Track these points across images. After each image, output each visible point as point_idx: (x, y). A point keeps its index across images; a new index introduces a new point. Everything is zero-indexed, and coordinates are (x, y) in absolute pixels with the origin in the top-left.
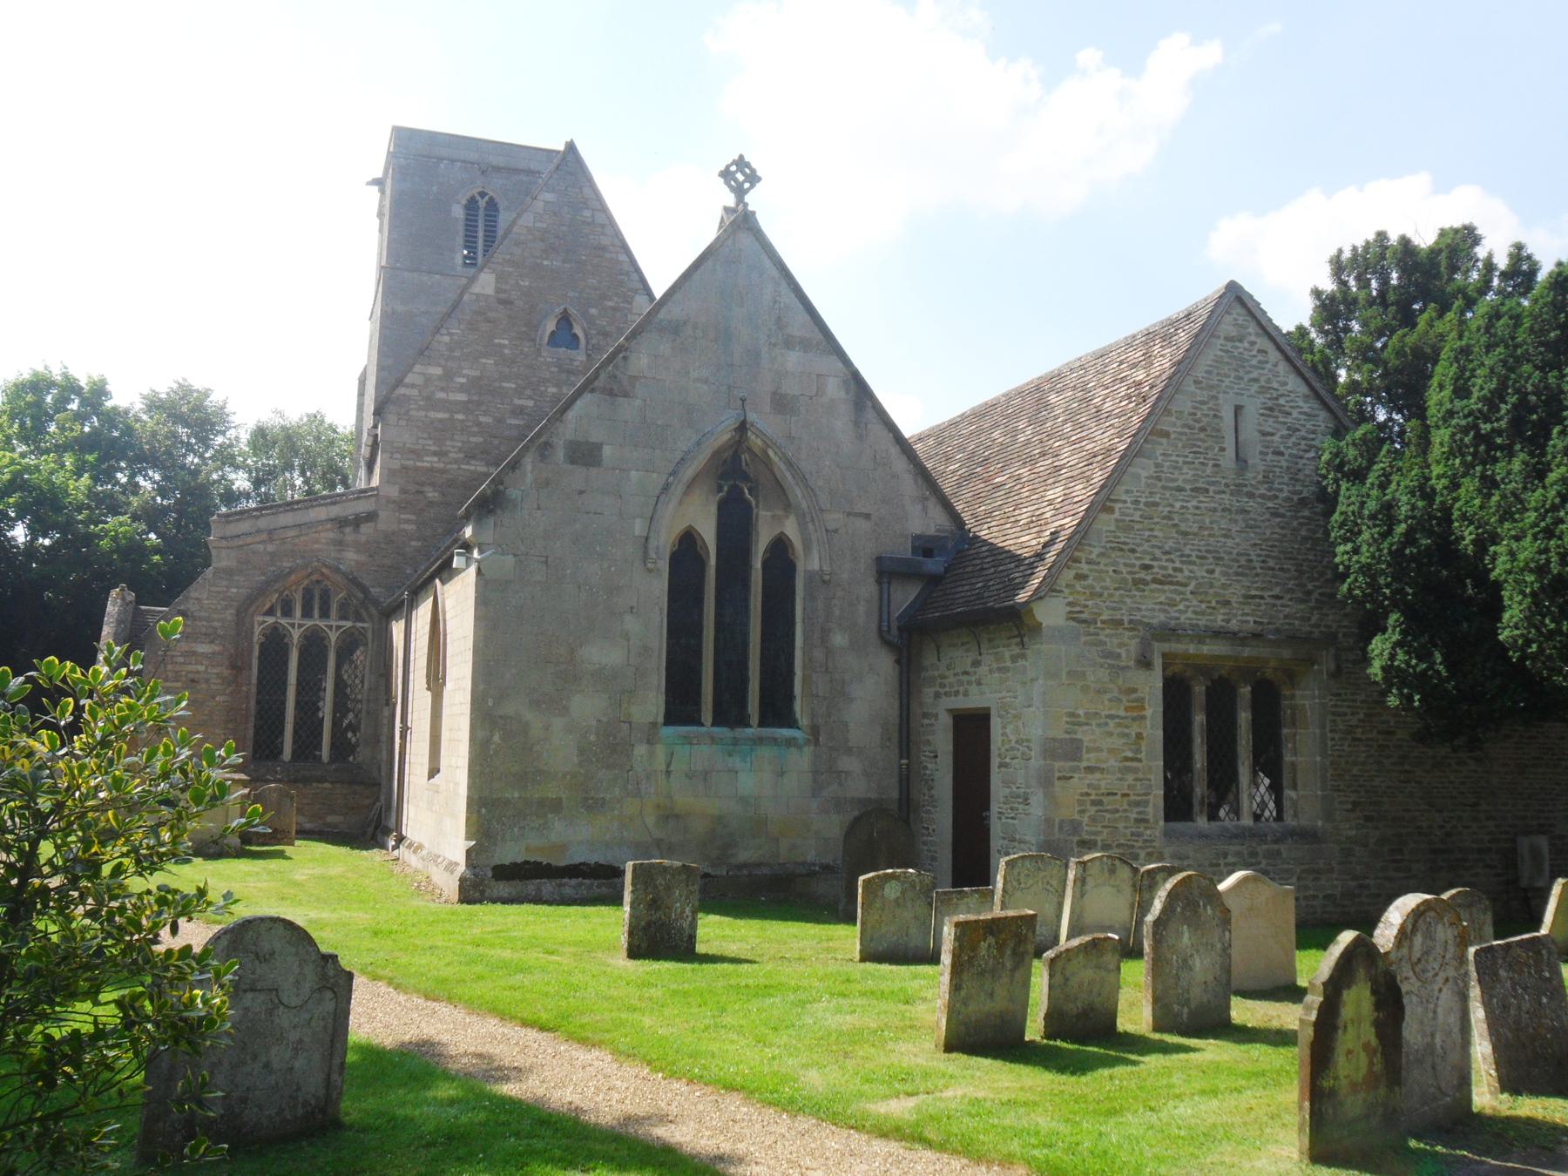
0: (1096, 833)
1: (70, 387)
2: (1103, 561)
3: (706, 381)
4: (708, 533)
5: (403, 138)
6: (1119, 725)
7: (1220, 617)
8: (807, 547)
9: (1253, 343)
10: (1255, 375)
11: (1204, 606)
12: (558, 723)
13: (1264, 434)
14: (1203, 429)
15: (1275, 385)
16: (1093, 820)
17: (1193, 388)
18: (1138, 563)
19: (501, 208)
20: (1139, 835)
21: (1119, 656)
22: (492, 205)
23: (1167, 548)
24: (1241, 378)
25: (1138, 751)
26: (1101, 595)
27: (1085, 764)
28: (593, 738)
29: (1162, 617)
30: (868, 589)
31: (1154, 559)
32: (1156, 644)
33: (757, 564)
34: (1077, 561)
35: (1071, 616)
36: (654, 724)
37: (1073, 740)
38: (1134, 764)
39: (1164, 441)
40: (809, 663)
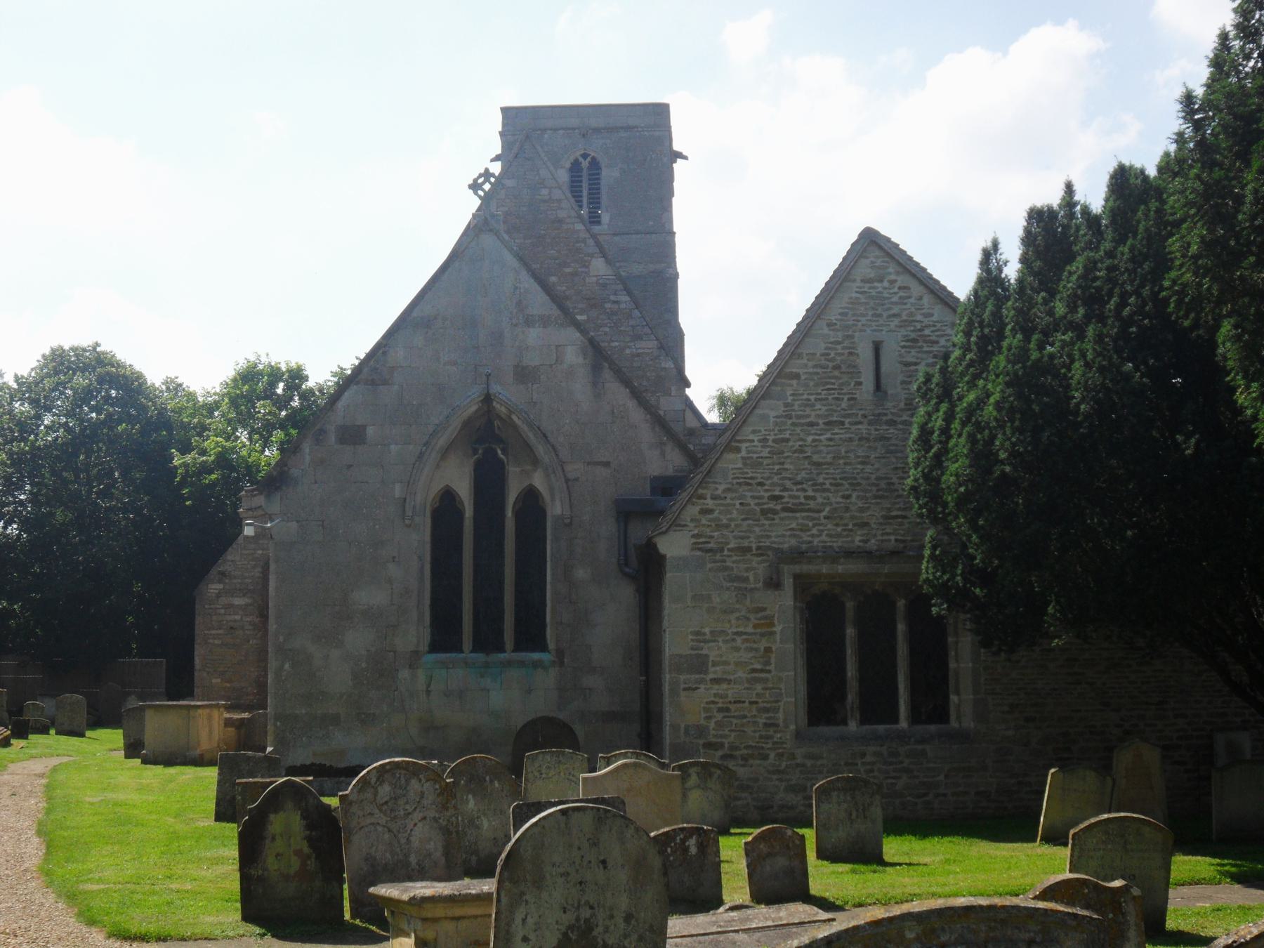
0: (721, 736)
1: (275, 374)
2: (729, 495)
3: (455, 364)
4: (464, 490)
5: (509, 114)
6: (747, 641)
7: (858, 538)
8: (553, 499)
9: (892, 282)
10: (896, 310)
11: (839, 529)
13: (907, 364)
14: (837, 367)
15: (919, 318)
16: (719, 725)
17: (826, 331)
18: (766, 495)
19: (603, 166)
20: (768, 737)
21: (746, 580)
22: (595, 164)
23: (799, 478)
24: (880, 315)
25: (768, 663)
26: (727, 526)
27: (711, 676)
28: (364, 665)
29: (793, 542)
30: (608, 528)
31: (785, 489)
32: (786, 567)
33: (509, 513)
34: (702, 497)
35: (695, 547)
37: (699, 656)
38: (763, 675)
39: (794, 382)
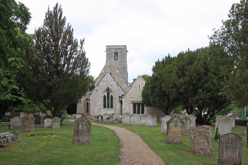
12: (96, 108)
30: (118, 98)
36: (102, 108)
40: (114, 104)
